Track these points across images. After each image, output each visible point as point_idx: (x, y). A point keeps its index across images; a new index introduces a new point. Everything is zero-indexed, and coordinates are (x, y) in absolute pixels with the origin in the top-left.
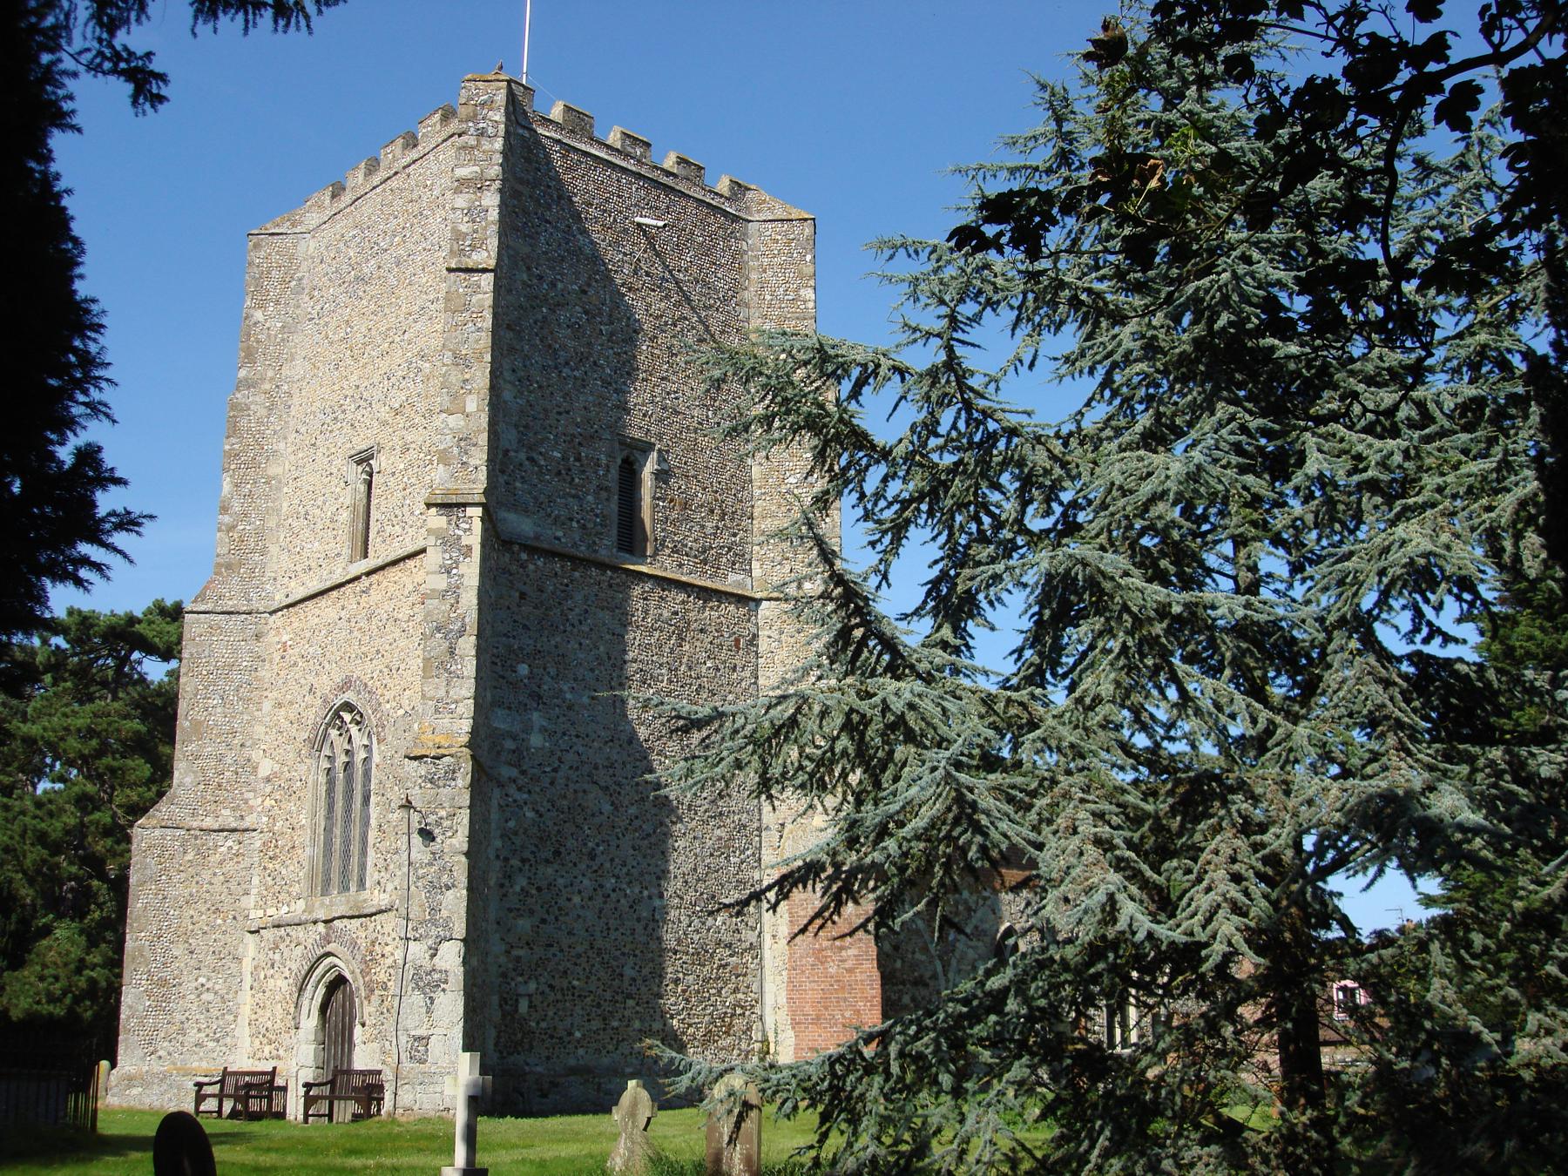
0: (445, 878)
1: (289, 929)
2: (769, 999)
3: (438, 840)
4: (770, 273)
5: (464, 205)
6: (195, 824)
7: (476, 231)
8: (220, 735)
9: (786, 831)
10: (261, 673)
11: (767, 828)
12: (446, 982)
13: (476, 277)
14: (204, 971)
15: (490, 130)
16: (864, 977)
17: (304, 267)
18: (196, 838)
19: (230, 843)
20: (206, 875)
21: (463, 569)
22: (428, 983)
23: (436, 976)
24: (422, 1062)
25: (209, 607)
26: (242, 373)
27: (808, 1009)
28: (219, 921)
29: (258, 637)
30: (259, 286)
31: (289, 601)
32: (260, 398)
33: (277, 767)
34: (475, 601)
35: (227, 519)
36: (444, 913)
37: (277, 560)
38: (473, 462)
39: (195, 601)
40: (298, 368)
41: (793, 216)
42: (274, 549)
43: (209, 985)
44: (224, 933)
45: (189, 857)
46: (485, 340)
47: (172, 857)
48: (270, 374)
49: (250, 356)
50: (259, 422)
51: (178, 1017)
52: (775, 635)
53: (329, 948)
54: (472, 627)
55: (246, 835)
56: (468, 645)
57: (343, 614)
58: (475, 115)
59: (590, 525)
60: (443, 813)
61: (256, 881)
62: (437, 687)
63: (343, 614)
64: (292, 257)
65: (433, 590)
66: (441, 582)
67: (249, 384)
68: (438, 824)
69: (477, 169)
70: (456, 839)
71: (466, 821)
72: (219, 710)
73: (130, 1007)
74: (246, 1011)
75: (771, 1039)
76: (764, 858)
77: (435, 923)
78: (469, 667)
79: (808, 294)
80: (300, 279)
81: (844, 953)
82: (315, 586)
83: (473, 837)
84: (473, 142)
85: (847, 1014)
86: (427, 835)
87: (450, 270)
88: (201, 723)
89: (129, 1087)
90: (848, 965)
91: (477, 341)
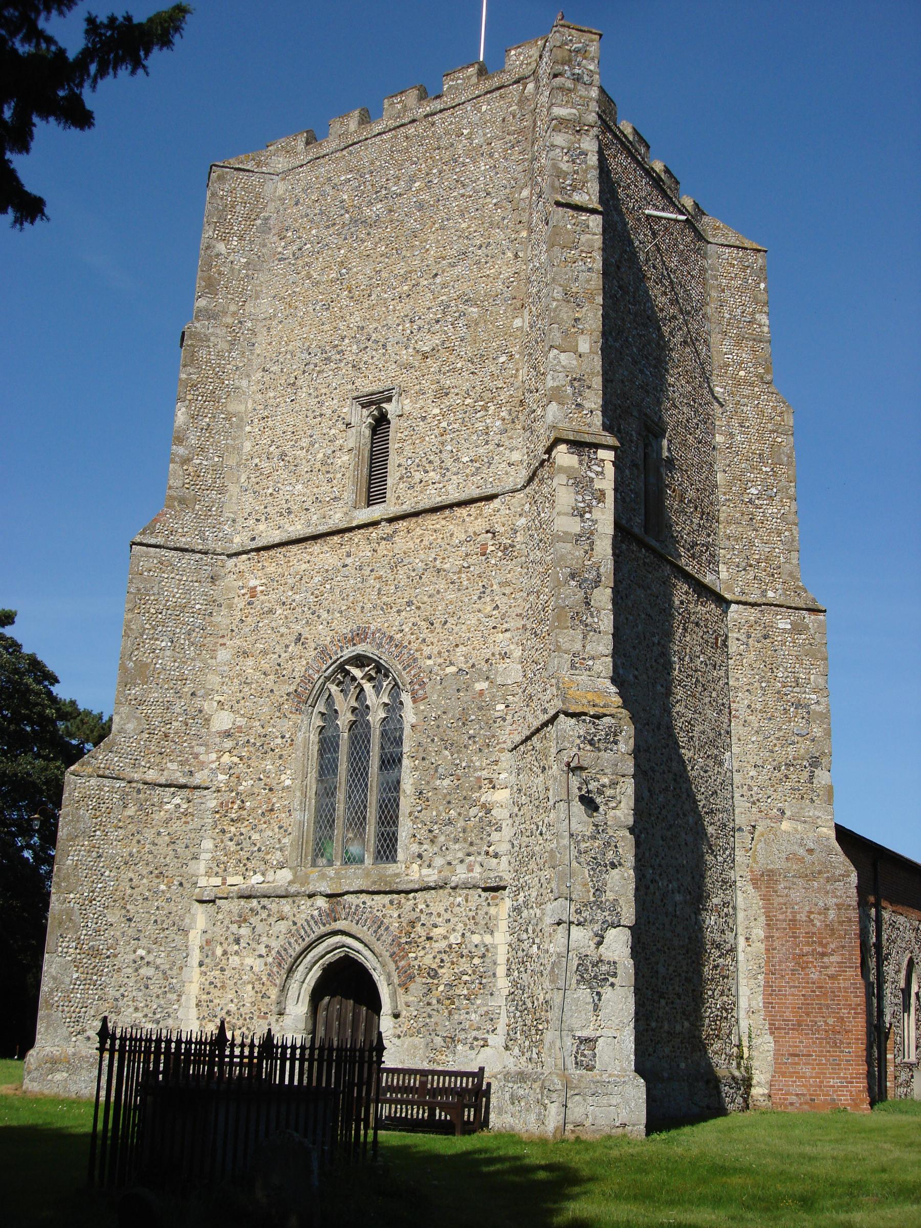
0: (610, 855)
1: (265, 901)
2: (743, 1003)
3: (602, 808)
4: (727, 293)
5: (564, 144)
6: (136, 776)
7: (576, 172)
8: (166, 680)
9: (757, 833)
10: (217, 619)
11: (740, 829)
12: (615, 975)
13: (584, 217)
14: (143, 942)
15: (586, 78)
16: (847, 984)
17: (271, 207)
18: (139, 791)
19: (177, 800)
20: (149, 834)
21: (597, 514)
22: (594, 975)
23: (604, 968)
24: (590, 1068)
25: (160, 540)
26: (202, 303)
27: (788, 1014)
28: (163, 887)
29: (213, 579)
30: (222, 219)
31: (254, 545)
32: (222, 331)
33: (241, 721)
34: (610, 551)
35: (181, 450)
36: (610, 896)
37: (239, 500)
38: (588, 405)
39: (143, 533)
40: (264, 306)
41: (746, 245)
42: (233, 489)
43: (150, 958)
44: (169, 900)
45: (131, 811)
46: (596, 282)
47: (110, 811)
48: (233, 308)
49: (211, 287)
50: (220, 356)
51: (111, 993)
52: (743, 638)
53: (338, 925)
54: (608, 578)
55: (197, 792)
56: (603, 597)
57: (349, 561)
58: (570, 61)
59: (628, 500)
60: (605, 780)
61: (208, 844)
62: (571, 640)
63: (349, 561)
64: (258, 196)
65: (565, 533)
66: (574, 526)
67: (211, 315)
68: (600, 792)
69: (574, 111)
70: (621, 810)
71: (630, 790)
72: (168, 653)
73: (55, 979)
74: (193, 989)
75: (745, 1043)
76: (737, 858)
77: (600, 906)
78: (606, 622)
79: (764, 319)
80: (267, 219)
81: (826, 959)
82: (298, 529)
83: (639, 810)
84: (569, 84)
85: (831, 1021)
86: (589, 803)
87: (558, 204)
88: (147, 665)
89: (51, 1071)
90: (832, 971)
91: (588, 281)
